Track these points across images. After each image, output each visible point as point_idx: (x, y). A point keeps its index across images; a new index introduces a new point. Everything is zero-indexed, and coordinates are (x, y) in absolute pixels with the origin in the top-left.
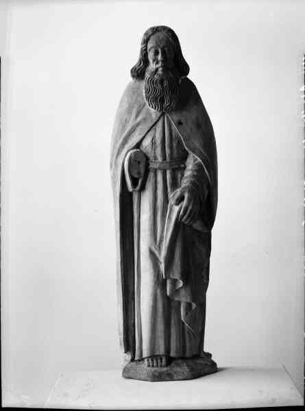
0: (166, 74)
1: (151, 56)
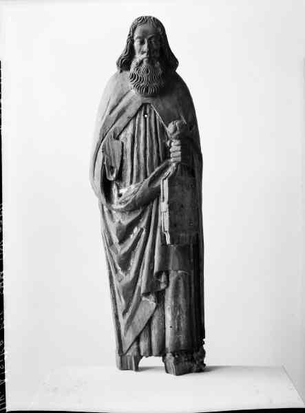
0: (154, 63)
1: (136, 44)
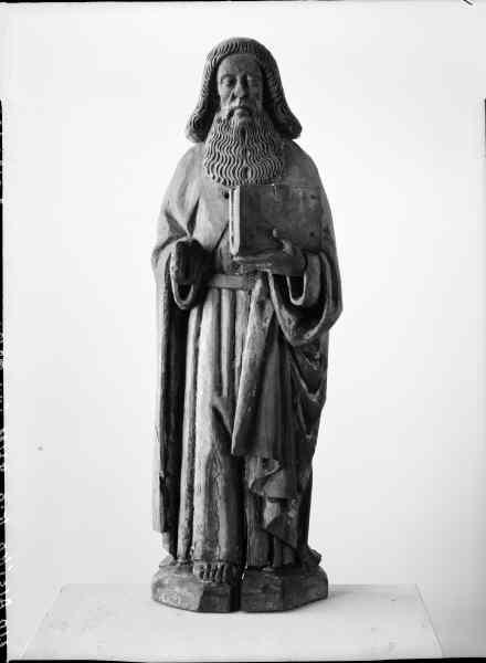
0: (250, 105)
1: (222, 89)
